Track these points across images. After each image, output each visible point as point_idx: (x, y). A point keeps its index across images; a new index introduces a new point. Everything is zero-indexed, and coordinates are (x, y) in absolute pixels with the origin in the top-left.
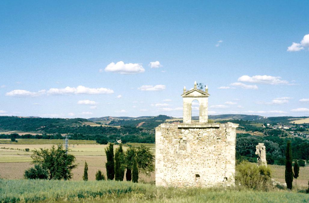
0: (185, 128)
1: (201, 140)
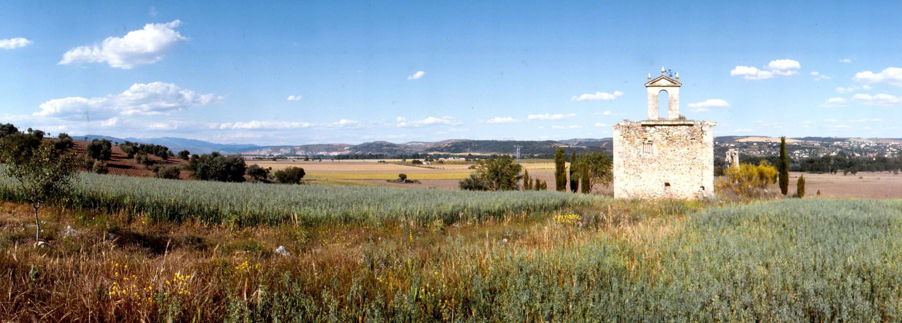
0: (651, 126)
1: (671, 141)
